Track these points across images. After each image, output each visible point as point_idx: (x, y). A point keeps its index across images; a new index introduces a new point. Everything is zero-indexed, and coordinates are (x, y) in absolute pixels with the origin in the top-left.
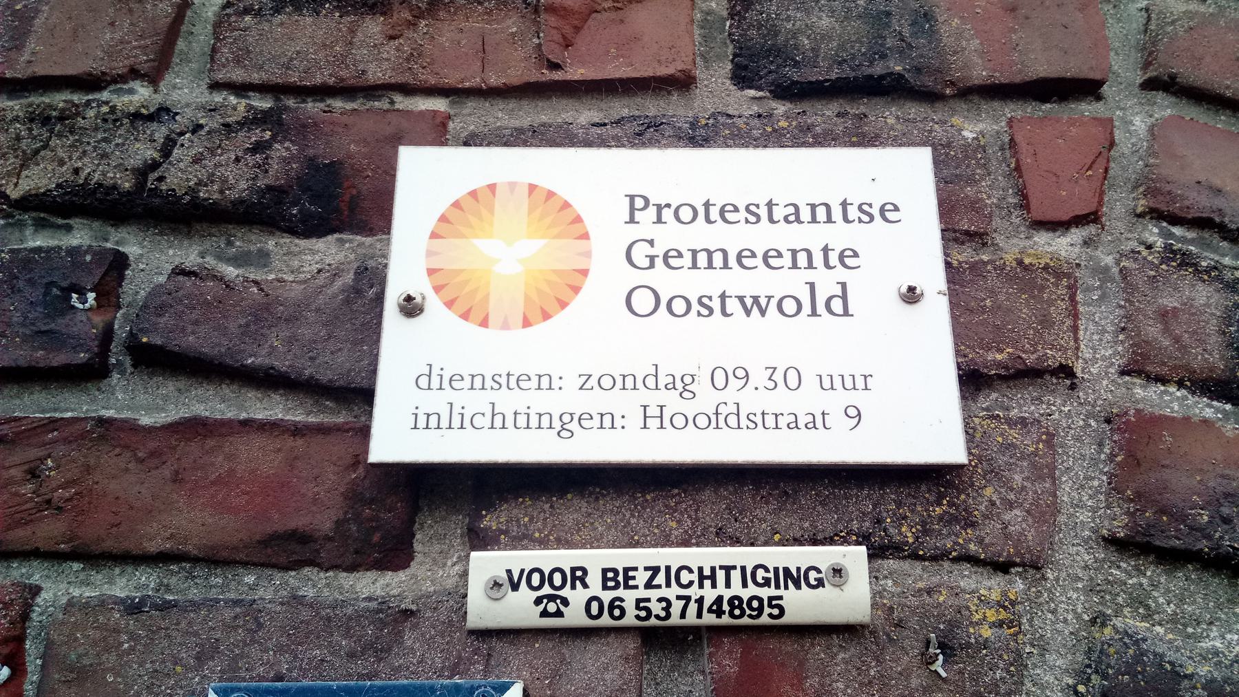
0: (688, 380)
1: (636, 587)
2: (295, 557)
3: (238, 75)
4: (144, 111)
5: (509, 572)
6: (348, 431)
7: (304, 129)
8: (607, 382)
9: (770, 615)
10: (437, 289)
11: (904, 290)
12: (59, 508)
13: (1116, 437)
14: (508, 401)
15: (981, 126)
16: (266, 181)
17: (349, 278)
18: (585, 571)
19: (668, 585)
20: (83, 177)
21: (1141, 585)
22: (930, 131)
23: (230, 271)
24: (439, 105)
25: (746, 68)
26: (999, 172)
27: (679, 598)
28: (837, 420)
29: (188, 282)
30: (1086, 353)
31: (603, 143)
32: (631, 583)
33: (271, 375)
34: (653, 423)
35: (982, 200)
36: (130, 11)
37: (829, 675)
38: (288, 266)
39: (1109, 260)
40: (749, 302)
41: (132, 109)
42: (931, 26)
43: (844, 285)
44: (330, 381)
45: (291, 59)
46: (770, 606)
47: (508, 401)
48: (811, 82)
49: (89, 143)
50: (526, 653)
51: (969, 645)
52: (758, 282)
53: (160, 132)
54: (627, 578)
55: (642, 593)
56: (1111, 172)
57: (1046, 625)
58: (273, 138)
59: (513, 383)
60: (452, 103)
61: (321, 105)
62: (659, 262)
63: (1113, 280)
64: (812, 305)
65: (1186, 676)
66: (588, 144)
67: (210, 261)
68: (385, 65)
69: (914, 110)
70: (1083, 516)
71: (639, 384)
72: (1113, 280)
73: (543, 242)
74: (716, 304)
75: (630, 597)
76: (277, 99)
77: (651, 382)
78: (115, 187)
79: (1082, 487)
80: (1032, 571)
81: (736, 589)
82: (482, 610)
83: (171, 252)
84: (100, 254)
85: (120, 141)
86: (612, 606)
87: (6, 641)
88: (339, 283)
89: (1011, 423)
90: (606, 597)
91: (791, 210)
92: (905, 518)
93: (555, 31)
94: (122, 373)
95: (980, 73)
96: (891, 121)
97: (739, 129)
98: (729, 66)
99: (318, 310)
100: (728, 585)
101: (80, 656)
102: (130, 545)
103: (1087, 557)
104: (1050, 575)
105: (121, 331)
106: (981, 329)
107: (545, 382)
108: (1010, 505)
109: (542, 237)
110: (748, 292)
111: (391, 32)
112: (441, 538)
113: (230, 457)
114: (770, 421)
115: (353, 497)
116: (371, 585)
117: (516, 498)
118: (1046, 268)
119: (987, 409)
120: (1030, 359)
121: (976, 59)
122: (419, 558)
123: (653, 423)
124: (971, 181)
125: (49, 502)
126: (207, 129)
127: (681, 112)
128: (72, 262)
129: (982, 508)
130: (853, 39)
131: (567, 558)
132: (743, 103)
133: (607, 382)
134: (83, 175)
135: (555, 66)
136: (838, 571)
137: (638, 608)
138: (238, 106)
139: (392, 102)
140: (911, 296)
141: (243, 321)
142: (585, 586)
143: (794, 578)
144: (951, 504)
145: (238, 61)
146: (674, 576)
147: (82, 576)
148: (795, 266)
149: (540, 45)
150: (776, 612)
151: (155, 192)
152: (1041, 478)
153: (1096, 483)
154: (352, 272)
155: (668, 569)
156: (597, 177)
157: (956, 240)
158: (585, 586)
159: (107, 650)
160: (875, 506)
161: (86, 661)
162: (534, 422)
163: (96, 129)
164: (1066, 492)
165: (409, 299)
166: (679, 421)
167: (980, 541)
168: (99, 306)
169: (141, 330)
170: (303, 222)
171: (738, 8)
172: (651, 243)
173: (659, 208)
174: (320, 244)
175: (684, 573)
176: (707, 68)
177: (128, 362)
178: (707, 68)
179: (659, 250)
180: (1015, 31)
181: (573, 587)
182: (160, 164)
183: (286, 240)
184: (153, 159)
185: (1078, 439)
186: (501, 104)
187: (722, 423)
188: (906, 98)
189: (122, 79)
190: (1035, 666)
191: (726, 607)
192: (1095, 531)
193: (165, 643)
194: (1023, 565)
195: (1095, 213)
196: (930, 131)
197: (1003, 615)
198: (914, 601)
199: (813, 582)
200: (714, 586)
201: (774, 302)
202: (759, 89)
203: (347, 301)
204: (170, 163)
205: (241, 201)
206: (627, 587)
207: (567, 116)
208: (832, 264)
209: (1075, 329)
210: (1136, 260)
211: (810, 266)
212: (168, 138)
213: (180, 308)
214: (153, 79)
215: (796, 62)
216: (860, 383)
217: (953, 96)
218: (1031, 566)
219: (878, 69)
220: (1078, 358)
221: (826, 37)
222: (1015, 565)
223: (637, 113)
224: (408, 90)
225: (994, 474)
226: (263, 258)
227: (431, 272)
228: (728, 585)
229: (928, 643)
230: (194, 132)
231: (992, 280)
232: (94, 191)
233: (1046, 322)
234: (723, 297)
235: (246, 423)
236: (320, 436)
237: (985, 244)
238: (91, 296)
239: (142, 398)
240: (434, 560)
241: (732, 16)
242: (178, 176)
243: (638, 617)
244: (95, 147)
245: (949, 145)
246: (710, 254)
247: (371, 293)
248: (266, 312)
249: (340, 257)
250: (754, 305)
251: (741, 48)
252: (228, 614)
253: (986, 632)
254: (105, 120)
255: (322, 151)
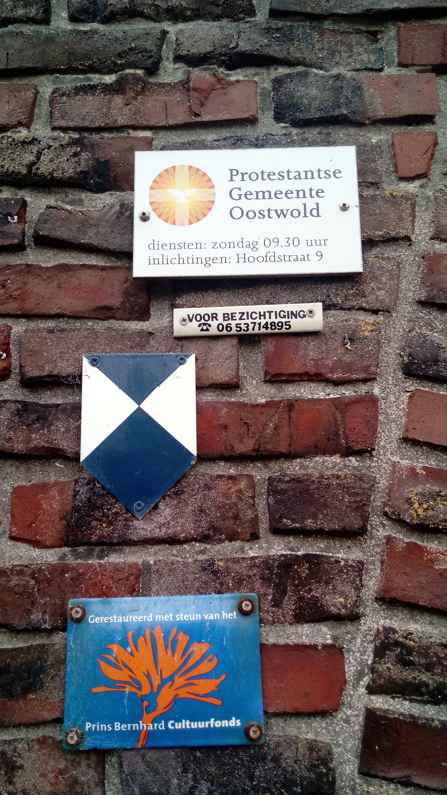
0: (255, 243)
1: (236, 320)
2: (107, 315)
3: (63, 123)
4: (27, 140)
5: (188, 315)
6: (122, 268)
7: (93, 146)
8: (223, 245)
9: (286, 328)
10: (154, 210)
11: (341, 205)
12: (15, 298)
13: (425, 263)
14: (185, 253)
15: (381, 137)
16: (80, 169)
17: (117, 208)
18: (216, 314)
19: (248, 318)
20: (6, 169)
21: (430, 318)
22: (357, 140)
23: (69, 207)
24: (148, 134)
25: (280, 113)
26: (387, 156)
27: (252, 323)
28: (313, 257)
29: (54, 211)
30: (417, 231)
31: (219, 148)
32: (234, 318)
33: (91, 247)
34: (241, 260)
35: (378, 169)
36: (15, 96)
37: (308, 350)
38: (91, 205)
39: (430, 193)
40: (279, 212)
41: (21, 139)
42: (361, 92)
43: (317, 204)
44: (114, 249)
45: (85, 116)
46: (286, 325)
47: (185, 253)
48: (307, 119)
49: (5, 155)
50: (196, 345)
51: (360, 338)
52: (283, 204)
53: (35, 149)
54: (232, 316)
55: (238, 322)
56: (436, 156)
57: (391, 333)
58: (81, 150)
59: (186, 247)
60: (154, 133)
61: (99, 136)
62: (243, 197)
63: (431, 202)
64: (305, 213)
65: (442, 348)
66: (212, 148)
67: (59, 203)
68: (125, 117)
69: (352, 131)
70: (410, 294)
71: (236, 246)
72: (431, 202)
73: (197, 189)
74: (266, 213)
75: (233, 323)
76: (80, 134)
77: (240, 245)
78: (19, 173)
79: (411, 283)
80: (387, 313)
81: (273, 319)
82: (179, 329)
83: (43, 200)
84: (17, 201)
85: (18, 153)
86: (227, 327)
87: (3, 344)
88: (113, 211)
89: (383, 259)
90: (225, 323)
91: (297, 174)
92: (339, 295)
93: (197, 99)
94: (31, 248)
95: (381, 114)
96: (341, 135)
97: (276, 141)
98: (273, 113)
99: (106, 221)
100: (270, 318)
101: (33, 347)
102: (43, 311)
103: (410, 309)
104: (394, 315)
105: (29, 232)
106: (374, 222)
107: (199, 246)
108: (380, 289)
109: (195, 188)
110: (279, 208)
111: (126, 102)
112: (160, 310)
113: (78, 279)
114: (287, 258)
115: (126, 293)
116: (135, 326)
117: (189, 293)
118: (402, 196)
119: (375, 255)
120: (393, 234)
121: (380, 107)
122: (152, 317)
123: (241, 260)
124: (374, 161)
125: (11, 296)
126: (54, 147)
127: (252, 134)
128: (7, 204)
129: (369, 290)
130: (326, 99)
131: (210, 310)
132: (279, 129)
133: (223, 245)
134: (6, 168)
135: (197, 115)
136: (311, 312)
137: (237, 327)
138: (66, 137)
139: (129, 134)
140: (344, 208)
141: (77, 226)
142: (217, 320)
143: (294, 315)
144: (356, 289)
145: (63, 118)
146: (250, 315)
147: (26, 324)
148: (298, 197)
149: (190, 106)
150: (288, 327)
151: (36, 174)
152: (393, 279)
153: (416, 282)
154: (118, 206)
155: (248, 313)
156: (216, 161)
157: (366, 186)
158: (217, 320)
159: (43, 345)
160: (327, 291)
161: (36, 349)
162: (195, 261)
163: (8, 149)
164: (404, 285)
165: (144, 214)
166: (251, 259)
167: (367, 302)
168: (19, 222)
169: (39, 229)
170: (95, 186)
171: (277, 86)
172: (240, 189)
173: (243, 174)
174: (102, 196)
175: (254, 314)
176: (263, 114)
177: (33, 244)
178: (263, 114)
179: (243, 192)
180: (397, 94)
181: (212, 320)
182: (36, 163)
183: (89, 194)
184: (33, 161)
185: (410, 265)
186: (174, 133)
187: (268, 260)
188: (349, 126)
189: (15, 126)
190: (385, 347)
191: (269, 326)
192: (413, 299)
193: (64, 343)
194: (383, 311)
195: (426, 173)
196: (357, 140)
197: (374, 327)
198: (340, 324)
199: (302, 316)
200: (265, 318)
201: (289, 212)
202: (286, 123)
203: (118, 218)
204: (41, 162)
205: (71, 178)
206: (232, 319)
207: (202, 137)
208: (313, 196)
209: (413, 222)
210: (441, 193)
211: (304, 197)
212: (38, 151)
213: (53, 221)
214: (28, 126)
215: (302, 110)
216: (323, 243)
217: (370, 124)
218: (386, 311)
219: (336, 113)
220: (413, 233)
221: (315, 99)
222: (380, 311)
223: (233, 135)
224: (135, 128)
225: (375, 278)
226: (80, 202)
227: (151, 203)
228: (270, 318)
229: (345, 338)
230: (48, 149)
231: (380, 202)
232: (11, 174)
233: (400, 218)
234: (269, 210)
235: (83, 266)
236: (112, 271)
237: (378, 188)
238: (16, 217)
239: (40, 258)
240: (158, 317)
241: (274, 90)
242: (45, 167)
243: (237, 330)
244: (8, 156)
245: (365, 146)
246: (264, 193)
247: (127, 214)
248: (86, 222)
249: (112, 201)
250: (281, 213)
251: (278, 105)
252: (86, 333)
253: (367, 334)
254: (11, 145)
255: (101, 155)
